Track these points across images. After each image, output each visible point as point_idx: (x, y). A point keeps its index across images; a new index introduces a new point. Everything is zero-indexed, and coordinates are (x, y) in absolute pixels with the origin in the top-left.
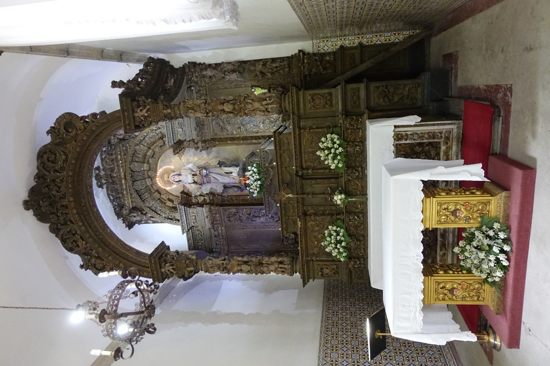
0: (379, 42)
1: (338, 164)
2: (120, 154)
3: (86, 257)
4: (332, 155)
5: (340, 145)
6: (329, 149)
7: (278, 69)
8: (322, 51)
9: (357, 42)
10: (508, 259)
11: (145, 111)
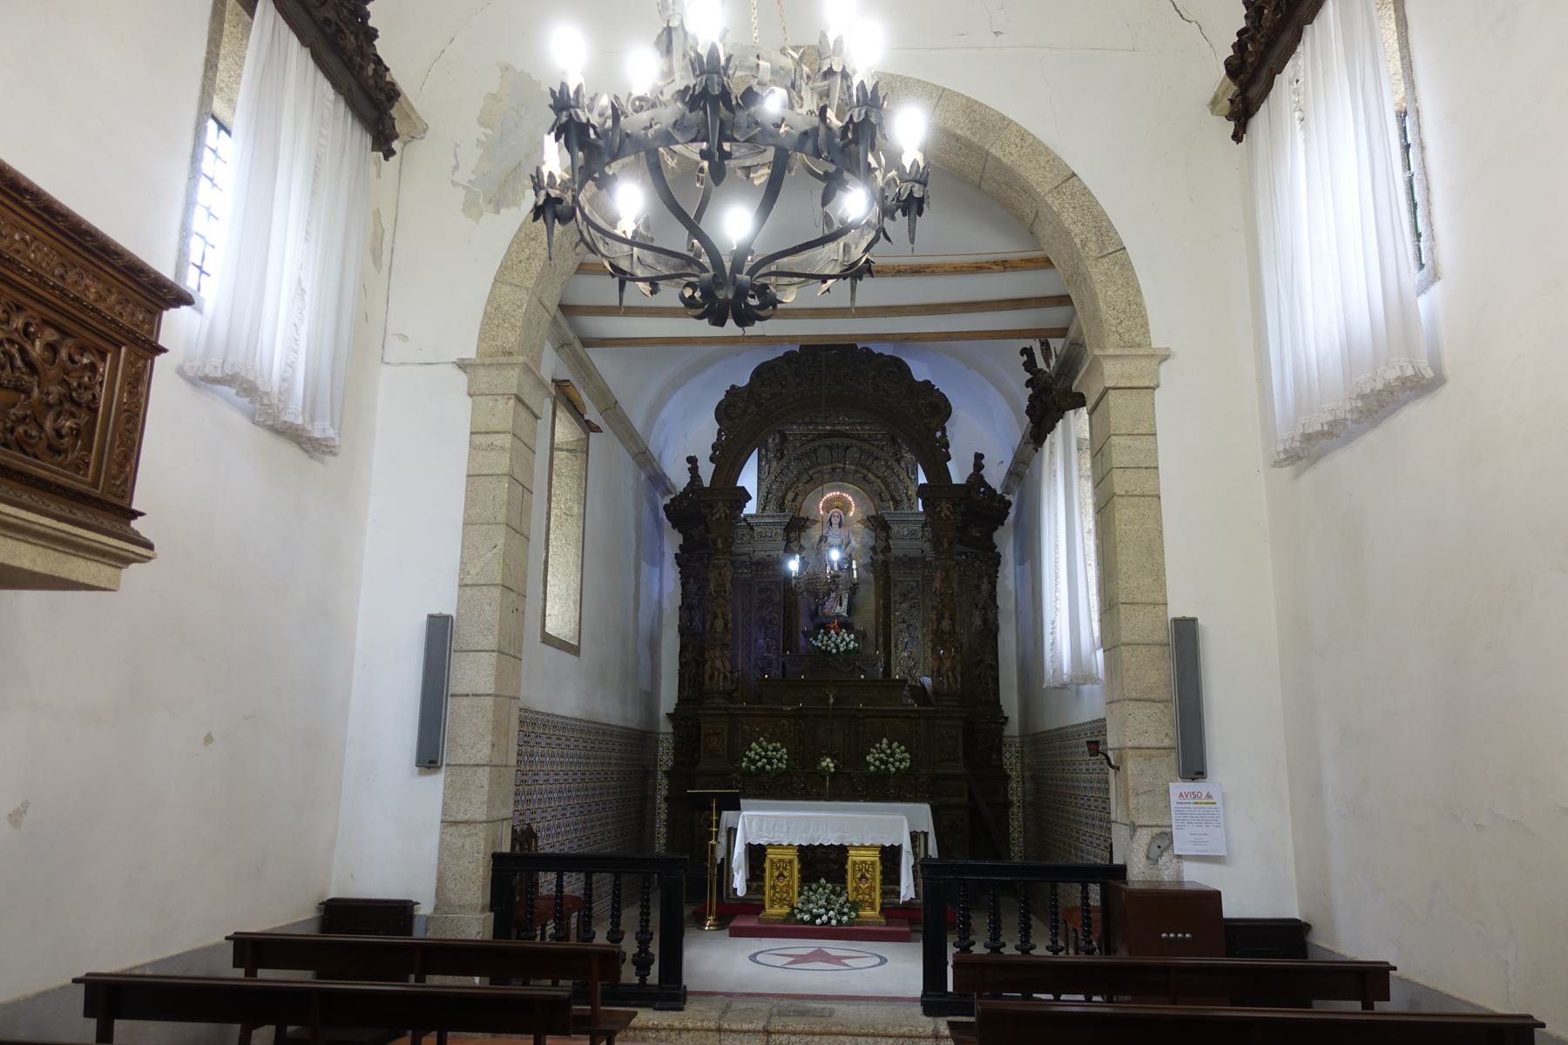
1: (874, 765)
2: (871, 430)
3: (746, 394)
4: (885, 758)
5: (898, 769)
6: (892, 756)
7: (984, 686)
8: (1004, 749)
10: (823, 924)
11: (948, 513)
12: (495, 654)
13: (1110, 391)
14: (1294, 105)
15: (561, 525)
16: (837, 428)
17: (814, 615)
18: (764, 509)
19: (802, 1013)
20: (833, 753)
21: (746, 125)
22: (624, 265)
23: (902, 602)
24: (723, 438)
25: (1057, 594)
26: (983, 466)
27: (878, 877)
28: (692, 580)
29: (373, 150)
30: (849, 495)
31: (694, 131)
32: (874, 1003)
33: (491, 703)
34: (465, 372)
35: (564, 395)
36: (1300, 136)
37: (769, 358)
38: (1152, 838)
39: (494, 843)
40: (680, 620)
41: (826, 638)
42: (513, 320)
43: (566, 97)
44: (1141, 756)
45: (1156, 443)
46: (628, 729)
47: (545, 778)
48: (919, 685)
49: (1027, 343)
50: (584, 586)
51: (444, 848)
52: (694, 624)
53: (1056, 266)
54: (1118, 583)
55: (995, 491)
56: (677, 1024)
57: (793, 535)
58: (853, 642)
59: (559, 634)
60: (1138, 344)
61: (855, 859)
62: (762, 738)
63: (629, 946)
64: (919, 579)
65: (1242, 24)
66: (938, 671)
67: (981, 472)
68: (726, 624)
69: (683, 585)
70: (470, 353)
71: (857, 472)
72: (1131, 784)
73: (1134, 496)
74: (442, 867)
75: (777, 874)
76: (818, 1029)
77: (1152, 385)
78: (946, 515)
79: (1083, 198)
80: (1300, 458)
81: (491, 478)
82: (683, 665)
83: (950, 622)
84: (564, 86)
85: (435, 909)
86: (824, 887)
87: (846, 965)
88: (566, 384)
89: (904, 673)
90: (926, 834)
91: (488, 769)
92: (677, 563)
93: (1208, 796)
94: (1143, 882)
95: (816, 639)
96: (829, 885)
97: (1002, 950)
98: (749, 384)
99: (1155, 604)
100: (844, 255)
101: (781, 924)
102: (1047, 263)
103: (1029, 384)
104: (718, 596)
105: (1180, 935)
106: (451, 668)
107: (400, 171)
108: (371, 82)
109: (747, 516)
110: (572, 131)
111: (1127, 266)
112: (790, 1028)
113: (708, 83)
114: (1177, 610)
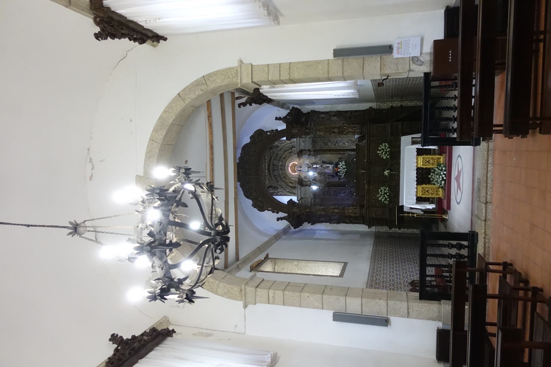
0: (411, 105)
1: (387, 156)
3: (255, 201)
4: (384, 152)
5: (388, 148)
6: (383, 150)
8: (381, 108)
9: (399, 104)
10: (446, 177)
11: (296, 130)
12: (347, 298)
13: (253, 81)
14: (154, 22)
15: (301, 268)
16: (266, 168)
17: (333, 176)
18: (295, 194)
19: (479, 190)
20: (382, 171)
21: (160, 236)
22: (209, 269)
23: (328, 145)
24: (270, 209)
25: (325, 94)
26: (280, 117)
27: (428, 156)
28: (321, 219)
29: (172, 337)
30: (290, 164)
31: (163, 253)
32: (475, 163)
33: (364, 299)
34: (248, 305)
35: (256, 268)
36: (165, 20)
37: (243, 193)
38: (414, 64)
39: (415, 299)
40: (335, 223)
41: (341, 173)
42: (230, 289)
43: (152, 297)
44: (384, 68)
45: (271, 64)
46: (374, 244)
47: (392, 277)
48: (358, 139)
49: (237, 106)
50: (323, 260)
51: (418, 317)
52: (336, 219)
53: (210, 99)
54: (321, 77)
55: (289, 113)
56: (483, 236)
58: (343, 163)
59: (340, 270)
60: (236, 71)
61: (421, 165)
62: (377, 196)
63: (454, 251)
64: (320, 139)
65: (127, 39)
66: (353, 133)
67: (282, 118)
68: (336, 208)
69: (322, 222)
70: (241, 303)
71: (282, 161)
72: (394, 72)
73: (290, 71)
74: (424, 319)
75: (427, 193)
76: (485, 185)
77: (251, 66)
78: (297, 131)
79: (187, 91)
80: (276, 15)
81: (284, 298)
82: (351, 223)
83: (335, 129)
84: (148, 297)
85: (440, 321)
86: (432, 176)
87: (461, 170)
88: (252, 267)
89: (354, 144)
90: (412, 138)
91: (388, 301)
92: (314, 224)
93: (398, 44)
94: (430, 67)
95: (341, 176)
96: (431, 174)
97: (455, 117)
98: (251, 200)
99: (328, 64)
100: (205, 193)
101: (446, 192)
102: (209, 102)
103: (251, 105)
104: (326, 211)
105: (450, 55)
106: (352, 313)
107: (179, 326)
108: (150, 337)
109: (298, 200)
110: (163, 294)
111: (210, 75)
112: (484, 195)
113: (146, 251)
114: (331, 56)
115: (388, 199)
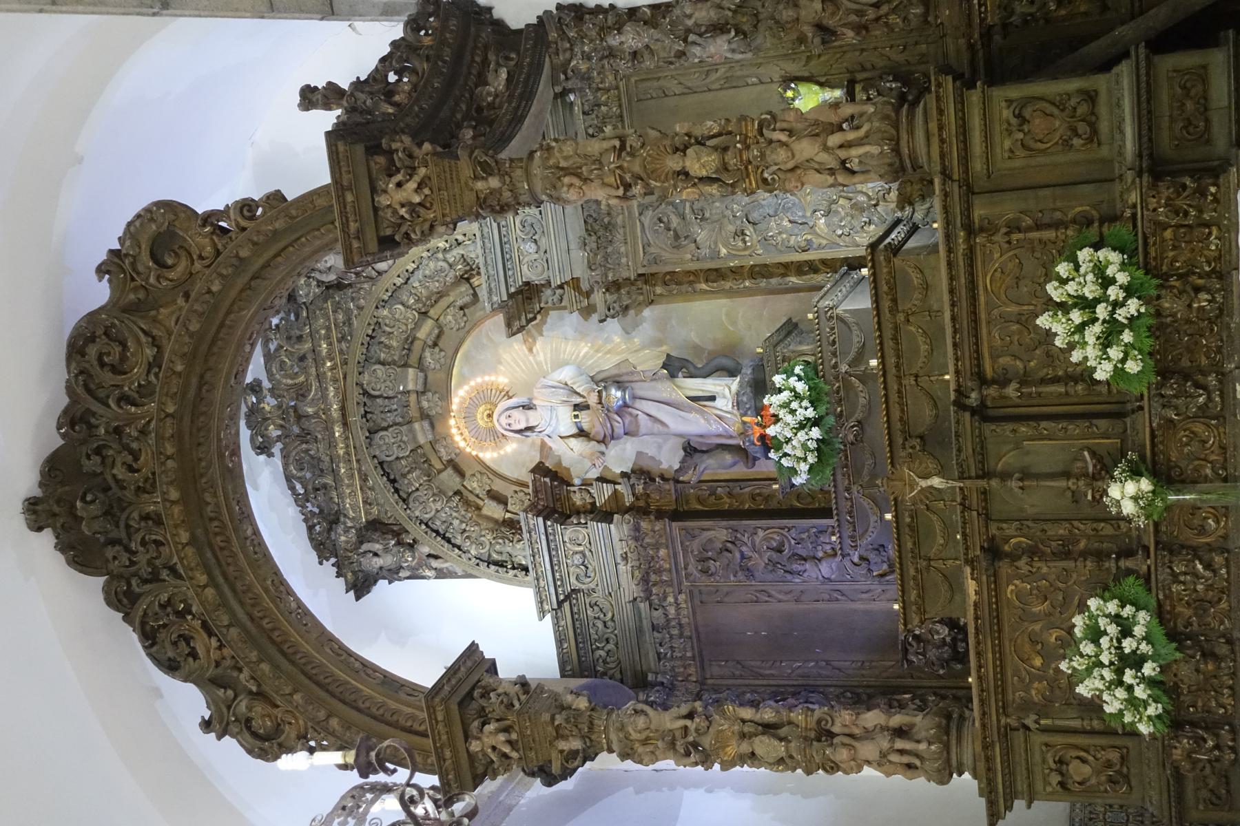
1: (1123, 361)
2: (328, 337)
3: (221, 692)
4: (1097, 328)
5: (1129, 291)
11: (412, 185)
57: (577, 499)
115: (1152, 710)
